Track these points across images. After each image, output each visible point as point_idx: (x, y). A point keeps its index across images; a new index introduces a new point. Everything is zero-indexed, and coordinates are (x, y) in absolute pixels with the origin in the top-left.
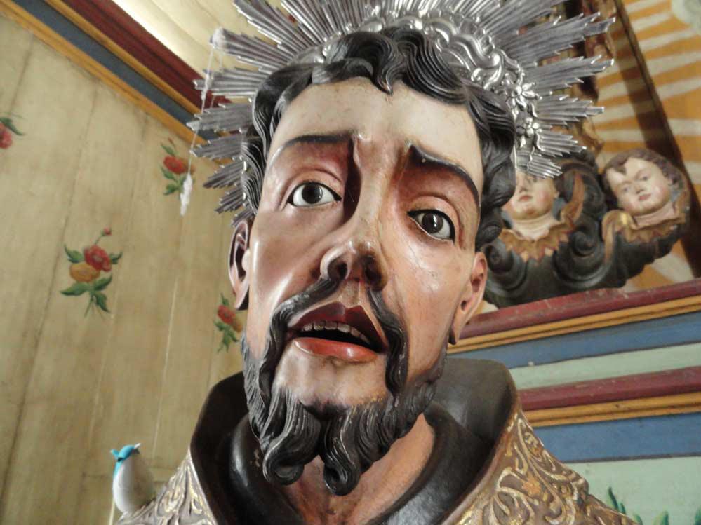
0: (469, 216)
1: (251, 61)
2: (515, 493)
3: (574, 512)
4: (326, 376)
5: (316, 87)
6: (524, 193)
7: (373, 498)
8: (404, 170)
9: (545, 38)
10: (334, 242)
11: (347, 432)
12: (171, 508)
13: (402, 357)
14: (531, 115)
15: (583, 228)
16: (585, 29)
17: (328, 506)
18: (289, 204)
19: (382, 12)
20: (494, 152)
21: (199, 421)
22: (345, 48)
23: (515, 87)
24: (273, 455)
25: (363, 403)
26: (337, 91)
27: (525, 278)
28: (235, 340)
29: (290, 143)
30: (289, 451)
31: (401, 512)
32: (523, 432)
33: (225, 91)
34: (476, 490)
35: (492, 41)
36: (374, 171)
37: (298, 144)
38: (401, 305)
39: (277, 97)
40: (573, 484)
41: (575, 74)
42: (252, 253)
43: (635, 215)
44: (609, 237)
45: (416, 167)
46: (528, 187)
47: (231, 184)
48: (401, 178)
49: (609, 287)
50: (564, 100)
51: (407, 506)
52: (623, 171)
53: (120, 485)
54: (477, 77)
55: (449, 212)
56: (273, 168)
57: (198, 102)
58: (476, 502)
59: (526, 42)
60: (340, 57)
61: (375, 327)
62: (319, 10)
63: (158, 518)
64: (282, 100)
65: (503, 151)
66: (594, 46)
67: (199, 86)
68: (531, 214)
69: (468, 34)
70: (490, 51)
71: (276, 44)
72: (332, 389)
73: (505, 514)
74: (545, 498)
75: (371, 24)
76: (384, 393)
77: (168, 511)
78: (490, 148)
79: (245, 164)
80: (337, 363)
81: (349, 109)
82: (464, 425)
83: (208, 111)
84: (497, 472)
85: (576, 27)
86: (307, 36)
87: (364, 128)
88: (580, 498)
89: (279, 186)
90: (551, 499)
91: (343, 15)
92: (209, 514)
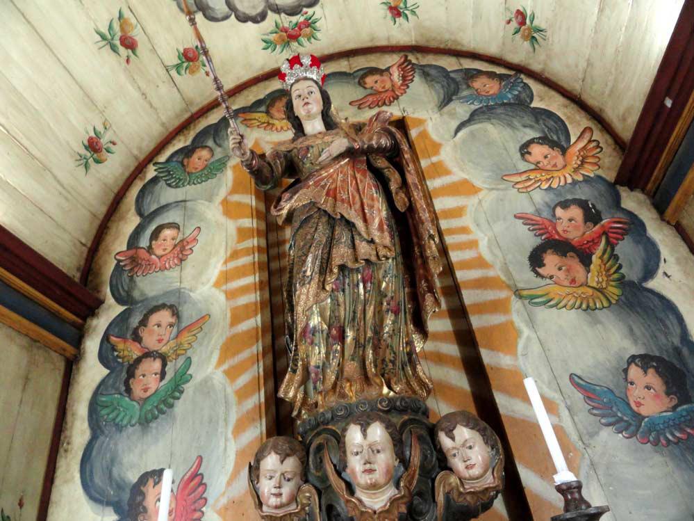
6: (368, 466)
7: (121, 431)
44: (440, 498)
46: (372, 460)
52: (453, 438)
68: (374, 487)
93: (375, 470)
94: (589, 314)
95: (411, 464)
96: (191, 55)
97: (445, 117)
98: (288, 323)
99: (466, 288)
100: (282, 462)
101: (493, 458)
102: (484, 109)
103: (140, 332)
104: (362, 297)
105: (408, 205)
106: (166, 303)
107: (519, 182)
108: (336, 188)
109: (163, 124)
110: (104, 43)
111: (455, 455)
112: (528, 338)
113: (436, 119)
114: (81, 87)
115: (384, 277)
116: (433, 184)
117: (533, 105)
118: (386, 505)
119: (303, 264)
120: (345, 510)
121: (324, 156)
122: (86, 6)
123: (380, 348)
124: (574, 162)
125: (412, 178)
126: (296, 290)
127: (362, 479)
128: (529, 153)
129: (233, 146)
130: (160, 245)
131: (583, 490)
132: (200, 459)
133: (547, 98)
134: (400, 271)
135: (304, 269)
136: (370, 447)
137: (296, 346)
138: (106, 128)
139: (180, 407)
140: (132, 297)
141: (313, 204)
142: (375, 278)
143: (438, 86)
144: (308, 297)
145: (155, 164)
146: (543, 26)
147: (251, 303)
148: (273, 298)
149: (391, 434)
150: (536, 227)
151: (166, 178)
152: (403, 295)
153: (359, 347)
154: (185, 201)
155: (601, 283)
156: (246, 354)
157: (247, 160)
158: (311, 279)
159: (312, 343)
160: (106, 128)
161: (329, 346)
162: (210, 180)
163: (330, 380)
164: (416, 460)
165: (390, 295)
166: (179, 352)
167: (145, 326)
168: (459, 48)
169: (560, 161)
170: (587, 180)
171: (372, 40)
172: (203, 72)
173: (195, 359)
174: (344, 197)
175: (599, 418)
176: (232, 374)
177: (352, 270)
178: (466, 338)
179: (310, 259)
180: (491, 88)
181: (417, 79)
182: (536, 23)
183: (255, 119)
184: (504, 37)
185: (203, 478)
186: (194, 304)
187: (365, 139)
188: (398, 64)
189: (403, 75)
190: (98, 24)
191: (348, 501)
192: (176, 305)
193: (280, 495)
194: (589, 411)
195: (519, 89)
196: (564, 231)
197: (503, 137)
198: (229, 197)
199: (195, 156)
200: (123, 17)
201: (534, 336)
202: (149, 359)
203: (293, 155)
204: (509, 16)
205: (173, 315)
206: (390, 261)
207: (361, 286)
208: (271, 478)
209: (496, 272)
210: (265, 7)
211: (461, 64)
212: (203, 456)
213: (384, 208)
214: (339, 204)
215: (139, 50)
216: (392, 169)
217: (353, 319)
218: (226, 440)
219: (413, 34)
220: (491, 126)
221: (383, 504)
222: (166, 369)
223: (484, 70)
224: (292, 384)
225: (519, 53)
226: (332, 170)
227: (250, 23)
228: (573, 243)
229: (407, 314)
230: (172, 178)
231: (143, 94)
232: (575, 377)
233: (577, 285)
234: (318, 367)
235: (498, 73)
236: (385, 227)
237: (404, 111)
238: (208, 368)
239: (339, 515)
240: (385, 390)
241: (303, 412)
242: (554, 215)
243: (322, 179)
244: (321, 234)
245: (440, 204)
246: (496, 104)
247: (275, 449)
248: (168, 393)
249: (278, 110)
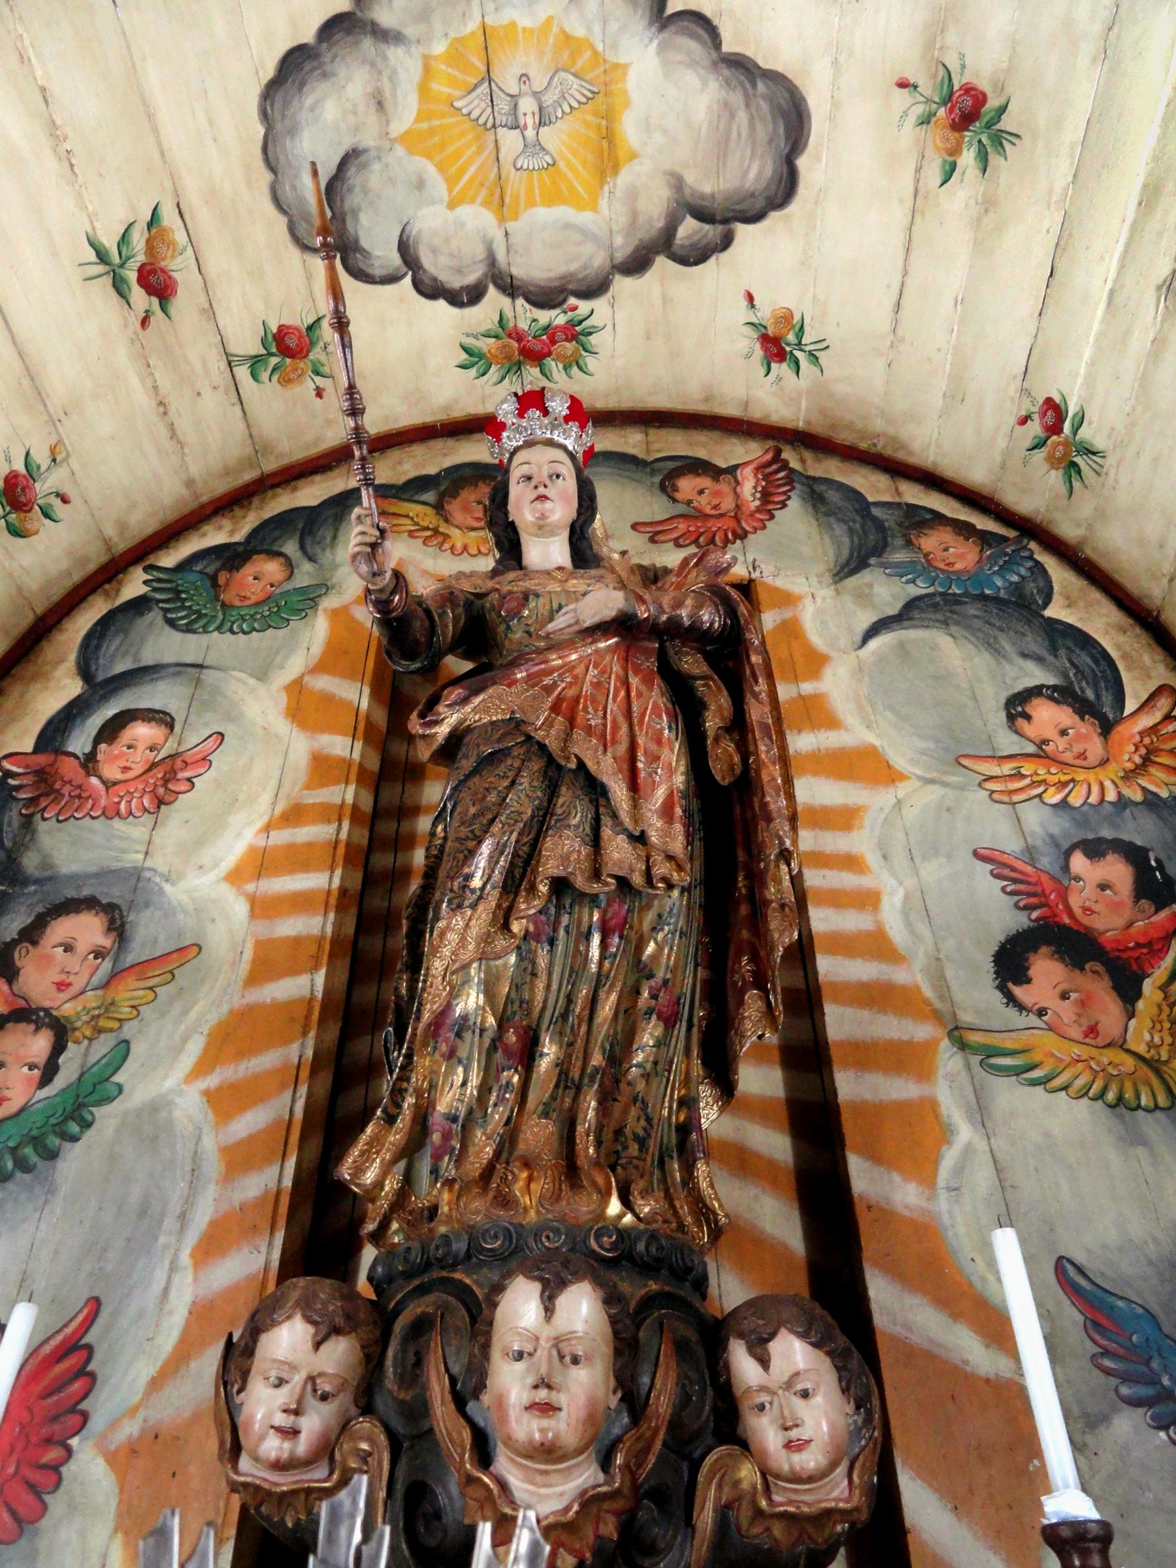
6: (542, 1394)
44: (706, 1518)
46: (557, 1380)
52: (764, 1362)
68: (547, 1453)
93: (560, 1409)
94: (1121, 1117)
95: (649, 1411)
96: (292, 342)
97: (847, 599)
98: (399, 997)
99: (836, 1000)
100: (317, 1345)
101: (855, 1434)
102: (938, 599)
103: (16, 955)
104: (594, 967)
105: (738, 770)
106: (98, 897)
107: (996, 777)
108: (577, 700)
109: (190, 483)
111: (762, 1408)
112: (968, 1150)
113: (824, 599)
115: (654, 929)
116: (801, 742)
117: (1048, 613)
118: (567, 1509)
119: (466, 857)
120: (458, 1504)
121: (560, 622)
122: (80, 179)
123: (615, 1100)
124: (1126, 757)
125: (757, 712)
126: (437, 918)
127: (526, 1428)
128: (1028, 718)
129: (357, 549)
130: (118, 757)
131: (1113, 1549)
132: (95, 1305)
133: (1081, 604)
134: (695, 925)
135: (466, 870)
136: (556, 1346)
137: (409, 1057)
138: (54, 460)
139: (75, 1162)
140: (19, 864)
141: (515, 725)
142: (631, 927)
143: (840, 530)
144: (463, 939)
145: (147, 569)
146: (1099, 443)
147: (309, 937)
148: (361, 940)
149: (613, 1321)
150: (1021, 887)
151: (168, 606)
152: (689, 982)
153: (566, 1087)
154: (201, 666)
155: (1158, 1047)
156: (266, 1060)
157: (381, 591)
158: (480, 898)
159: (451, 1055)
160: (54, 460)
161: (493, 1072)
162: (271, 630)
163: (477, 1155)
164: (663, 1403)
165: (660, 974)
166: (102, 1023)
167: (34, 943)
168: (901, 456)
169: (1095, 748)
170: (1151, 802)
171: (706, 400)
173: (138, 1049)
174: (593, 723)
175: (1114, 1381)
176: (224, 1102)
177: (583, 895)
178: (816, 1123)
179: (486, 848)
180: (961, 556)
181: (794, 503)
182: (1085, 433)
183: (407, 516)
184: (1007, 453)
185: (88, 1360)
186: (170, 912)
187: (666, 601)
190: (98, 225)
191: (471, 1480)
192: (124, 908)
193: (292, 1433)
194: (1094, 1357)
195: (1023, 571)
196: (1086, 910)
197: (973, 670)
198: (307, 679)
199: (249, 570)
200: (158, 220)
201: (981, 1145)
202: (23, 1025)
203: (488, 605)
204: (1026, 407)
205: (109, 930)
206: (676, 893)
207: (596, 939)
208: (280, 1383)
209: (910, 975)
210: (485, 275)
212: (103, 1299)
213: (682, 769)
214: (578, 734)
215: (181, 303)
216: (715, 683)
217: (564, 1016)
218: (173, 1268)
219: (804, 403)
220: (949, 639)
221: (558, 1505)
222: (60, 1061)
223: (949, 515)
224: (377, 1153)
225: (1034, 491)
226: (574, 657)
227: (442, 304)
228: (1101, 939)
229: (695, 1030)
230: (183, 608)
231: (161, 403)
232: (1068, 1266)
233: (1100, 1041)
234: (454, 1119)
235: (979, 527)
236: (678, 811)
237: (754, 568)
238: (165, 1077)
239: (437, 1515)
240: (614, 1207)
241: (395, 1226)
242: (1066, 868)
243: (549, 672)
244: (522, 797)
245: (812, 791)
246: (966, 594)
247: (307, 1309)
248: (53, 1121)
249: (476, 497)
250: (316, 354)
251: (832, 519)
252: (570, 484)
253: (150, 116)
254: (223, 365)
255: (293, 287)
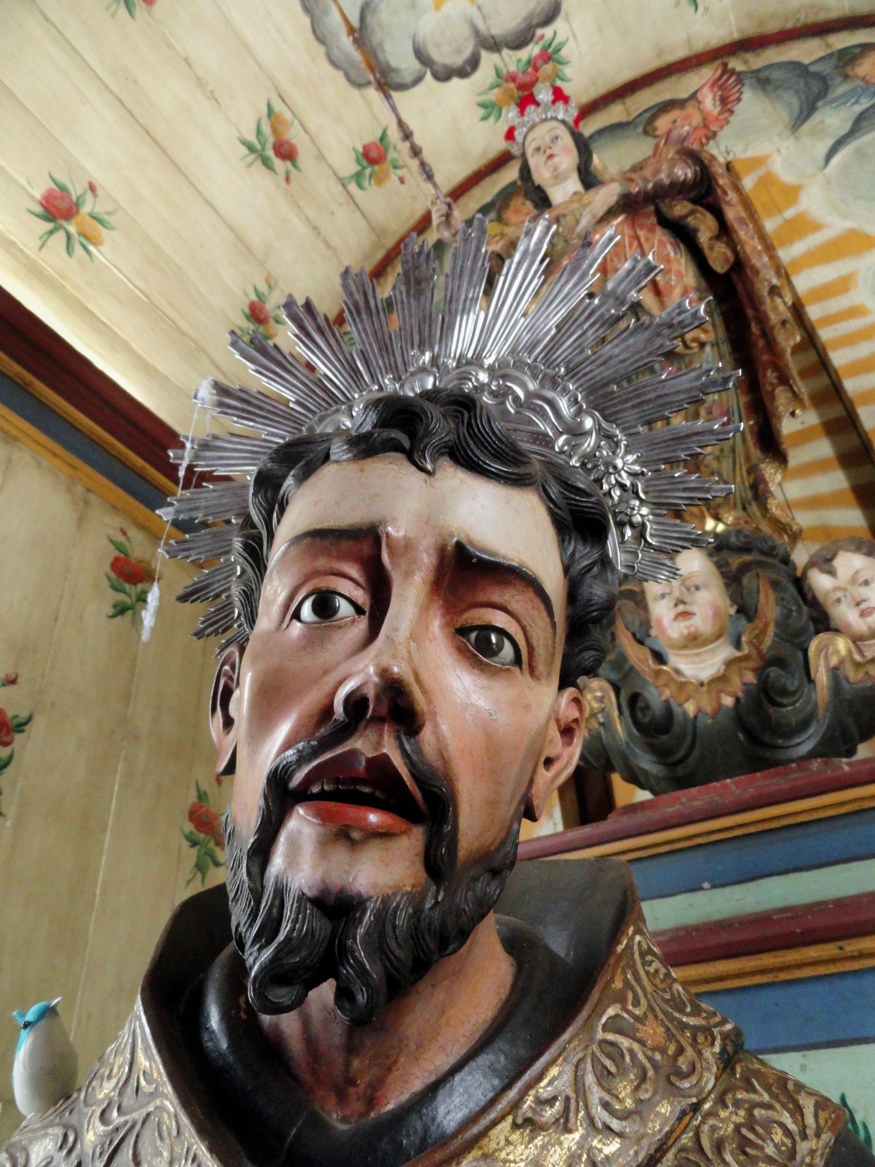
0: (540, 633)
1: (252, 424)
2: (625, 1043)
3: (715, 1069)
4: (340, 854)
5: (335, 466)
6: (681, 608)
8: (449, 573)
9: (652, 395)
10: (355, 669)
11: (367, 933)
12: (106, 1091)
13: (447, 828)
14: (638, 497)
15: (779, 662)
16: (702, 384)
17: (348, 1072)
18: (294, 621)
19: (434, 360)
20: (580, 547)
21: (155, 953)
22: (372, 417)
23: (615, 459)
24: (262, 969)
25: (390, 892)
26: (362, 471)
27: (693, 743)
28: (217, 864)
29: (298, 539)
30: (285, 961)
31: (457, 1078)
32: (643, 955)
33: (213, 465)
34: (566, 1036)
35: (582, 398)
36: (408, 575)
37: (308, 540)
38: (446, 756)
39: (284, 477)
40: (716, 1031)
41: (692, 442)
42: (242, 694)
43: (857, 640)
44: (822, 677)
45: (465, 571)
46: (687, 598)
47: (218, 596)
48: (445, 585)
49: (827, 756)
50: (679, 477)
51: (466, 1068)
52: (832, 573)
53: (24, 1067)
54: (563, 446)
55: (512, 628)
56: (275, 572)
57: (176, 481)
58: (565, 1054)
59: (627, 400)
60: (367, 427)
61: (408, 784)
62: (348, 357)
63: (85, 1110)
64: (289, 481)
65: (593, 547)
66: (774, 387)
67: (175, 458)
68: (694, 641)
69: (549, 389)
70: (579, 412)
71: (289, 400)
72: (348, 873)
73: (609, 1073)
74: (672, 1049)
75: (419, 376)
76: (423, 881)
77: (101, 1096)
78: (573, 543)
79: (239, 568)
80: (356, 835)
81: (376, 495)
82: (570, 960)
83: (187, 494)
84: (598, 1012)
85: (691, 381)
86: (330, 391)
87: (394, 519)
88: (724, 1050)
89: (282, 596)
90: (681, 1051)
91: (380, 362)
92: (168, 1089)
96: (373, 154)
105: (732, 260)
110: (253, 157)
111: (839, 601)
113: (787, 149)
114: (231, 228)
125: (732, 214)
160: (270, 287)
172: (396, 178)
188: (710, 83)
189: (721, 96)
206: (708, 349)
210: (475, 45)
211: (828, 46)
215: (304, 156)
219: (732, 18)
227: (456, 81)
240: (710, 524)
245: (803, 283)
250: (391, 155)
251: (779, 92)
252: (567, 140)
253: (245, 45)
254: (340, 187)
255: (362, 115)
